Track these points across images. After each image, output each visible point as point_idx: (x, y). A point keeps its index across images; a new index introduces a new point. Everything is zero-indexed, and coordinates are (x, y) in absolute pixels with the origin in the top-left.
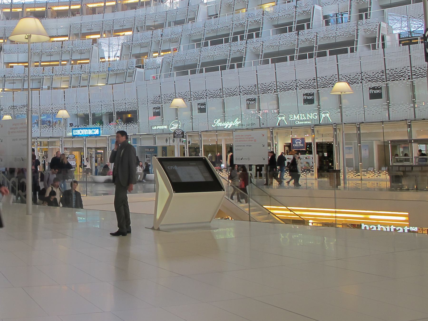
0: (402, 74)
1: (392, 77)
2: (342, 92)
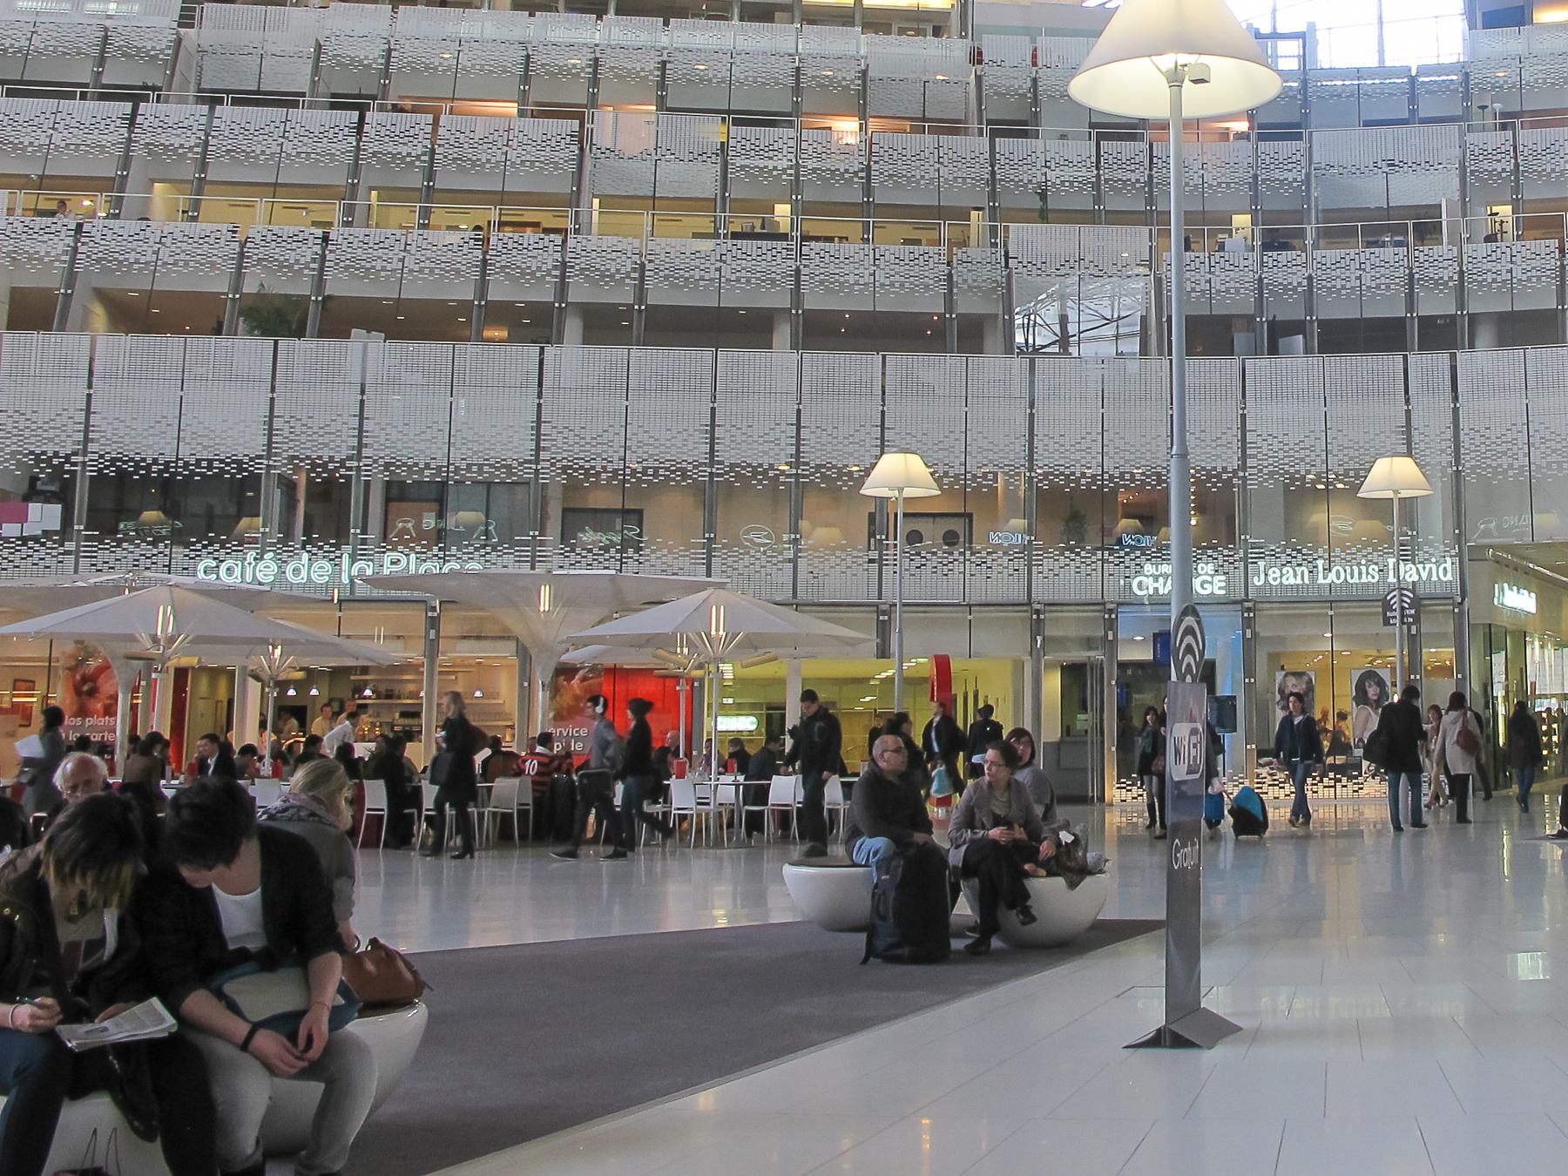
0: (51, 434)
1: (15, 439)
2: (1396, 492)
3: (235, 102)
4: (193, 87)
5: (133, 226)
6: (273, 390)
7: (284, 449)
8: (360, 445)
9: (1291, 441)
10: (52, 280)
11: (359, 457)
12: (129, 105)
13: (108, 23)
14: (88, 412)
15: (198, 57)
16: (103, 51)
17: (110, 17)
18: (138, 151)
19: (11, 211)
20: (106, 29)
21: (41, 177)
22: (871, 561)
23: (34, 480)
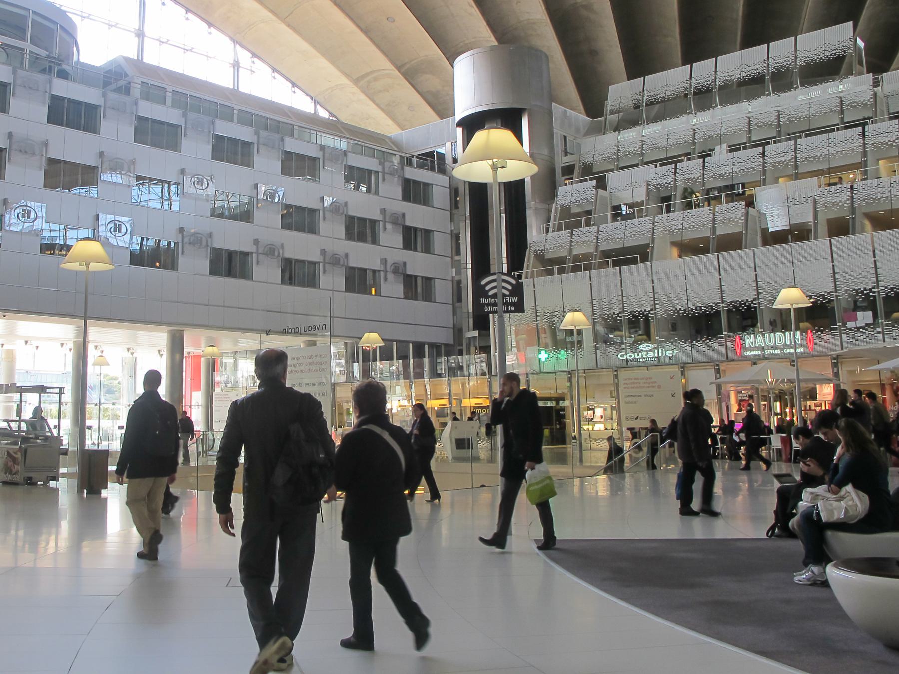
0: (861, 280)
3: (807, 136)
4: (885, 113)
5: (874, 182)
6: (832, 261)
7: (842, 287)
8: (877, 281)
9: (672, 296)
10: (845, 213)
11: (878, 287)
12: (860, 128)
13: (841, 95)
14: (757, 282)
15: (884, 100)
16: (842, 108)
17: (841, 92)
18: (869, 148)
19: (820, 186)
20: (778, 111)
21: (829, 169)
22: (879, 332)
23: (855, 302)
